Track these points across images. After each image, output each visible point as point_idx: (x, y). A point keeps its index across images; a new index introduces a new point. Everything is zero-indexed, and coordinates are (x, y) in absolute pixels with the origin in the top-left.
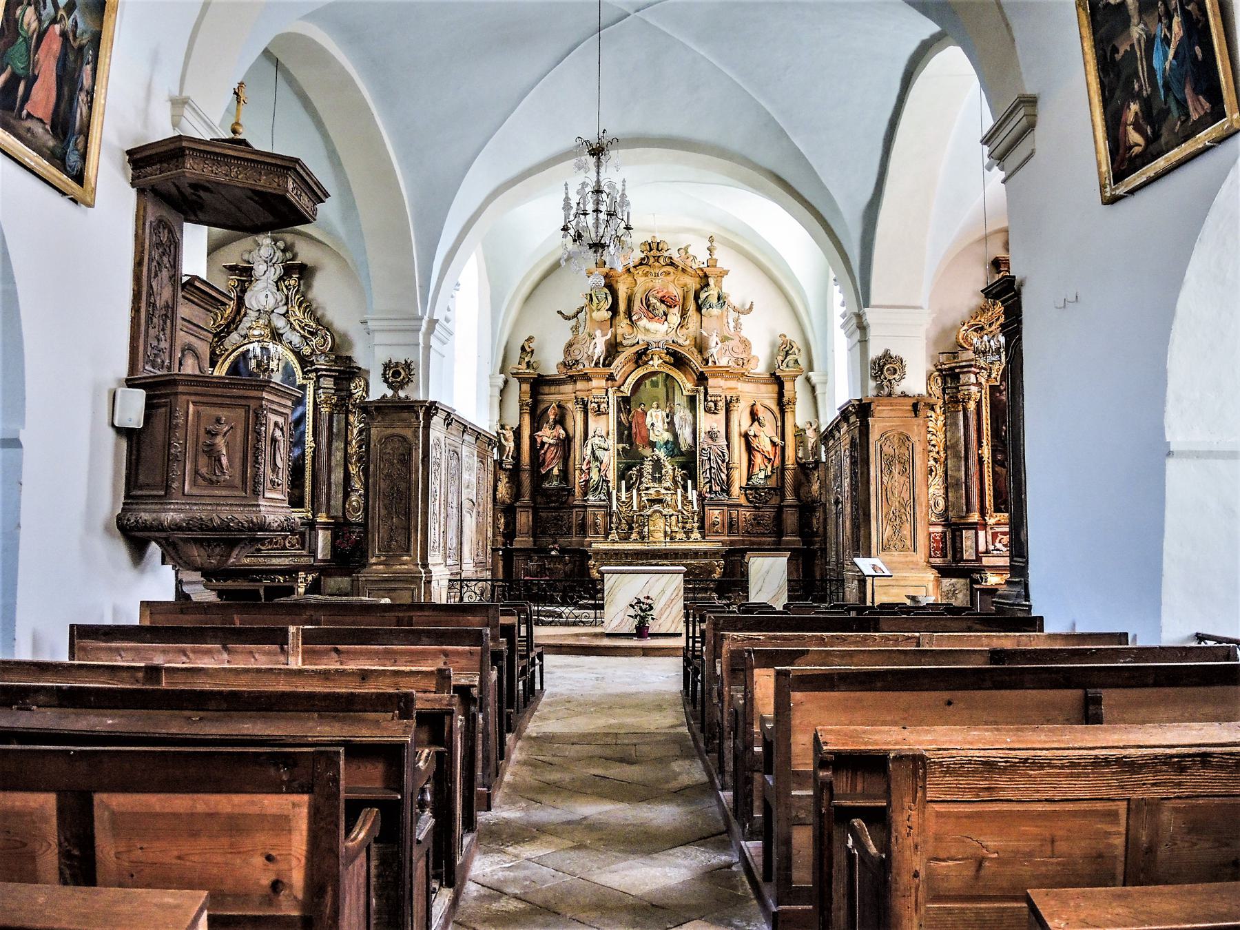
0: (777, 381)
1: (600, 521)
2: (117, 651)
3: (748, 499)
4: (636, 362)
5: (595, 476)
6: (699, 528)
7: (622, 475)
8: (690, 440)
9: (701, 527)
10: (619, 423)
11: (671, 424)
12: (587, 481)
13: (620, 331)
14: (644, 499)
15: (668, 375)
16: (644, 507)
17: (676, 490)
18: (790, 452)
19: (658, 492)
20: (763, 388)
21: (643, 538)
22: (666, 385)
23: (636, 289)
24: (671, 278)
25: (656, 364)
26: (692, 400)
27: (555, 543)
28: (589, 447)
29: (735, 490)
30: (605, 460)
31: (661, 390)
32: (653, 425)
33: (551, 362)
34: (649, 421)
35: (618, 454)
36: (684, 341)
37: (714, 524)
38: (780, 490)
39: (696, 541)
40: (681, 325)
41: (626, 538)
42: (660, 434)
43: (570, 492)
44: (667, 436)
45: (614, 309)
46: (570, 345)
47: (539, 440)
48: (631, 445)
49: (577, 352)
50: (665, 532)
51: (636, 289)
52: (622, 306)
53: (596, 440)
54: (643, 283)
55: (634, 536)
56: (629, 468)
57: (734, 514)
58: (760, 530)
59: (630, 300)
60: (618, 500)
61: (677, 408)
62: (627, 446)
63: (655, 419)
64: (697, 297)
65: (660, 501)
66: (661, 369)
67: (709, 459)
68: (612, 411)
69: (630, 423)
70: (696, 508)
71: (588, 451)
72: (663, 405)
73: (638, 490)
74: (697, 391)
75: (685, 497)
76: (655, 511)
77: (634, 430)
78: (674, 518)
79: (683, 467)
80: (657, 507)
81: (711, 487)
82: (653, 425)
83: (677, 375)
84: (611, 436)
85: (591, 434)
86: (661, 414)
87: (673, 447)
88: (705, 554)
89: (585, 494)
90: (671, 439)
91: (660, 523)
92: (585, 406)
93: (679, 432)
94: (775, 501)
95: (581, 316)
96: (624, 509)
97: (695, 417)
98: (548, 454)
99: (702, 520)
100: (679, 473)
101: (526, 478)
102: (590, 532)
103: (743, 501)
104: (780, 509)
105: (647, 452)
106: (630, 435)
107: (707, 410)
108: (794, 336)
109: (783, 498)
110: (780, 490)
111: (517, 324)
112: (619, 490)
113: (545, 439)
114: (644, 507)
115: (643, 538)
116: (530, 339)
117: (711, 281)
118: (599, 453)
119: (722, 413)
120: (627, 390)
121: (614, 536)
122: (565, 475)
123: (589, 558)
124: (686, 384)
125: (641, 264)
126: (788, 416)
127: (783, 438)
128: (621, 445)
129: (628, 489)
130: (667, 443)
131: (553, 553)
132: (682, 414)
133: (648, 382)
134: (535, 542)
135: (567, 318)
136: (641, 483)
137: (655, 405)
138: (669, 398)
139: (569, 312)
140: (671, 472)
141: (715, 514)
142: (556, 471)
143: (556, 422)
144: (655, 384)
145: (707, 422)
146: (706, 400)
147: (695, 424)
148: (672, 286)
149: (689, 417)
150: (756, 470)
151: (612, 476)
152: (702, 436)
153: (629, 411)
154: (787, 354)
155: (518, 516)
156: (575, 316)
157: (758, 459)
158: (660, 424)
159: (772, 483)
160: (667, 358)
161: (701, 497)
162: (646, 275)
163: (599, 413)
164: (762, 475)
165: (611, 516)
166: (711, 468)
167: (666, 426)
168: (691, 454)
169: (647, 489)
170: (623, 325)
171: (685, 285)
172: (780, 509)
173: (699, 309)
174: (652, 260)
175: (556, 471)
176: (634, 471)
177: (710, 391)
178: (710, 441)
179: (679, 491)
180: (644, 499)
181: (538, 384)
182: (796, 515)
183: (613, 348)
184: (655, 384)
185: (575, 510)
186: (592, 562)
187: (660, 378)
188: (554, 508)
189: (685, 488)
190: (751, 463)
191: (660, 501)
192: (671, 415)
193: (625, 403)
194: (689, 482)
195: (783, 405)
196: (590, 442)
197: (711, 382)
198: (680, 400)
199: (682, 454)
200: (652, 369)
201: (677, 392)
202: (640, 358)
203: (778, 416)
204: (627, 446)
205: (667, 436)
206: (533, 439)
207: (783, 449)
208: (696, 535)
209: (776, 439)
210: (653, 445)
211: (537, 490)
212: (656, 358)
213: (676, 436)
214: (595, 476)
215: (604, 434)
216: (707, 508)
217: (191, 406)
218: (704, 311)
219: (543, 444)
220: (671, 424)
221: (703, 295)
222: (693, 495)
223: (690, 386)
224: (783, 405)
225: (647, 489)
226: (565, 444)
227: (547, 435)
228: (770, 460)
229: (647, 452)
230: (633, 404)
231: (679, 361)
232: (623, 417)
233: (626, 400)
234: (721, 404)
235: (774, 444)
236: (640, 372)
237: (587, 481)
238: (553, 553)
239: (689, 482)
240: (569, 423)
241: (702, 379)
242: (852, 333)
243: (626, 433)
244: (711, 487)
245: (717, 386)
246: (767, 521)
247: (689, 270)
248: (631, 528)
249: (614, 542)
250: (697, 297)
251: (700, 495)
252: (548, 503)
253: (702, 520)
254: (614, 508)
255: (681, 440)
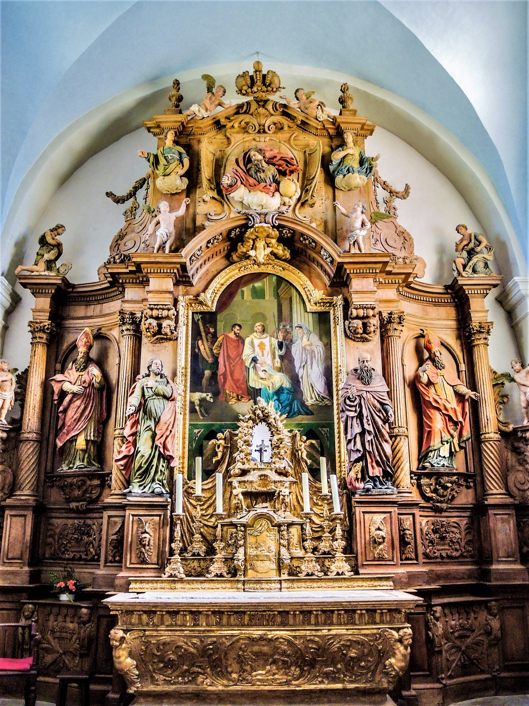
0: (457, 297)
1: (151, 536)
2: (356, 520)
3: (422, 494)
4: (228, 257)
5: (144, 447)
6: (345, 551)
7: (197, 449)
8: (320, 386)
9: (349, 550)
10: (196, 357)
11: (287, 359)
12: (130, 458)
13: (201, 209)
14: (238, 491)
15: (280, 280)
16: (238, 508)
17: (298, 475)
18: (489, 413)
19: (264, 477)
20: (435, 312)
21: (233, 572)
22: (277, 296)
23: (229, 150)
24: (283, 136)
25: (261, 252)
26: (323, 319)
27: (69, 576)
28: (138, 392)
29: (405, 478)
30: (166, 417)
31: (269, 305)
32: (254, 360)
33: (87, 269)
34: (247, 353)
35: (193, 411)
36: (310, 221)
37: (375, 542)
38: (474, 478)
39: (340, 577)
40: (302, 202)
41: (198, 574)
42: (268, 377)
43: (104, 480)
44: (280, 380)
45: (192, 175)
46: (121, 237)
47: (56, 388)
48: (216, 394)
49: (130, 244)
50: (279, 562)
51: (229, 150)
52: (206, 172)
53: (151, 382)
54: (239, 143)
55: (217, 567)
56: (211, 435)
57: (408, 522)
58: (444, 550)
59: (219, 166)
60: (188, 493)
61: (296, 333)
62: (209, 397)
63: (259, 349)
64: (326, 161)
65: (269, 496)
66: (269, 269)
67: (360, 416)
68: (184, 332)
69: (216, 359)
70: (337, 509)
71: (135, 400)
72: (272, 326)
73: (227, 475)
74: (331, 304)
75: (316, 491)
76: (261, 516)
77: (221, 369)
78: (295, 531)
79: (310, 433)
80: (262, 508)
81: (364, 471)
82: (254, 360)
83: (297, 278)
84: (179, 378)
85: (143, 370)
86: (270, 342)
87: (290, 398)
88: (372, 611)
89: (128, 483)
90: (287, 385)
91: (269, 541)
92: (136, 324)
93: (301, 373)
94: (465, 497)
95: (141, 193)
96: (197, 513)
97: (328, 346)
98: (71, 413)
99: (350, 535)
100: (303, 446)
101: (28, 453)
102: (129, 559)
103: (415, 496)
104: (479, 511)
105: (244, 407)
106: (214, 376)
107: (351, 335)
108: (473, 229)
109: (482, 492)
110: (474, 478)
111: (43, 213)
112: (191, 476)
113: (67, 387)
114: (238, 508)
115: (233, 572)
116: (58, 229)
117: (349, 138)
118: (155, 405)
119: (376, 338)
120: (210, 299)
121: (176, 567)
122: (99, 449)
123: (113, 622)
124: (312, 290)
125: (238, 113)
126: (479, 353)
127: (473, 385)
128: (197, 396)
129: (208, 474)
130: (279, 392)
131: (65, 598)
132: (306, 342)
133: (246, 290)
134: (34, 577)
135: (119, 200)
136: (233, 461)
137: (258, 326)
138: (283, 316)
139: (122, 191)
140: (287, 442)
141: (374, 523)
142: (81, 443)
143: (88, 360)
144: (258, 294)
145: (348, 355)
146: (346, 317)
147: (328, 358)
148: (290, 146)
149: (318, 346)
150: (436, 442)
151: (178, 448)
152: (342, 380)
153: (215, 337)
154: (471, 253)
155: (7, 523)
156: (132, 194)
157: (438, 422)
158: (268, 359)
159: (459, 465)
160: (280, 250)
161: (348, 491)
162: (245, 130)
163: (160, 336)
164: (445, 451)
165: (173, 525)
166: (362, 434)
167: (278, 363)
168: (325, 409)
169: (244, 473)
170: (205, 203)
171: (307, 146)
172: (479, 511)
173: (330, 179)
174: (254, 106)
175: (81, 443)
176: (220, 441)
177: (356, 300)
178: (359, 385)
179: (306, 476)
180: (238, 491)
181: (65, 298)
182: (512, 522)
183: (187, 231)
184: (258, 294)
185: (106, 514)
186: (117, 633)
187: (266, 285)
188: (77, 511)
189: (315, 473)
190: (424, 432)
191: (269, 496)
192: (285, 345)
193: (206, 323)
194: (323, 460)
195: (467, 334)
196: (138, 385)
197: (356, 284)
198: (302, 319)
199: (308, 412)
200: (255, 269)
201: (297, 307)
202: (234, 242)
203: (459, 354)
204: (209, 397)
205: (280, 380)
206: (46, 387)
207: (475, 405)
208: (340, 565)
209: (463, 389)
210: (254, 394)
211: (47, 478)
212: (260, 244)
213: (295, 380)
214: (144, 447)
215: (167, 372)
216: (358, 510)
217: (131, 517)
218: (339, 179)
219: (63, 394)
220: (287, 359)
221: (337, 156)
222: (330, 484)
223: (318, 294)
224: (467, 334)
225: (244, 473)
226: (103, 395)
227: (71, 380)
228: (456, 423)
229: (244, 407)
230: (220, 325)
231: (297, 249)
232: (204, 347)
233: (209, 318)
234: (375, 322)
235: (460, 397)
236: (232, 274)
237: (130, 458)
238: (65, 598)
239: (323, 460)
240: (113, 361)
241: (340, 281)
242: (514, 285)
243: (203, 373)
244: (364, 471)
245: (364, 291)
246: (456, 535)
247: (313, 123)
248: (211, 551)
249: (174, 580)
250: (326, 161)
251: (343, 485)
252: (68, 501)
253: (350, 535)
254: (179, 511)
255: (305, 387)
